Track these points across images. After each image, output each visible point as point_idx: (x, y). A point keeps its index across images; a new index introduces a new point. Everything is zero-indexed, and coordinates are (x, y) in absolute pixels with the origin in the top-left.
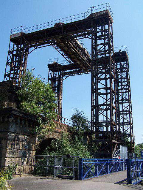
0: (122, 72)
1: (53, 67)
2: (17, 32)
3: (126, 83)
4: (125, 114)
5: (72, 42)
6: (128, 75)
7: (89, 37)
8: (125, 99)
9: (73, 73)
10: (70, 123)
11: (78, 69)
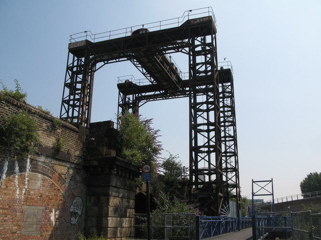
0: (224, 97)
1: (126, 88)
2: (80, 38)
3: (230, 113)
4: (228, 156)
5: (159, 56)
6: (233, 102)
7: (183, 50)
8: (227, 135)
9: (154, 97)
10: (162, 171)
11: (161, 92)
